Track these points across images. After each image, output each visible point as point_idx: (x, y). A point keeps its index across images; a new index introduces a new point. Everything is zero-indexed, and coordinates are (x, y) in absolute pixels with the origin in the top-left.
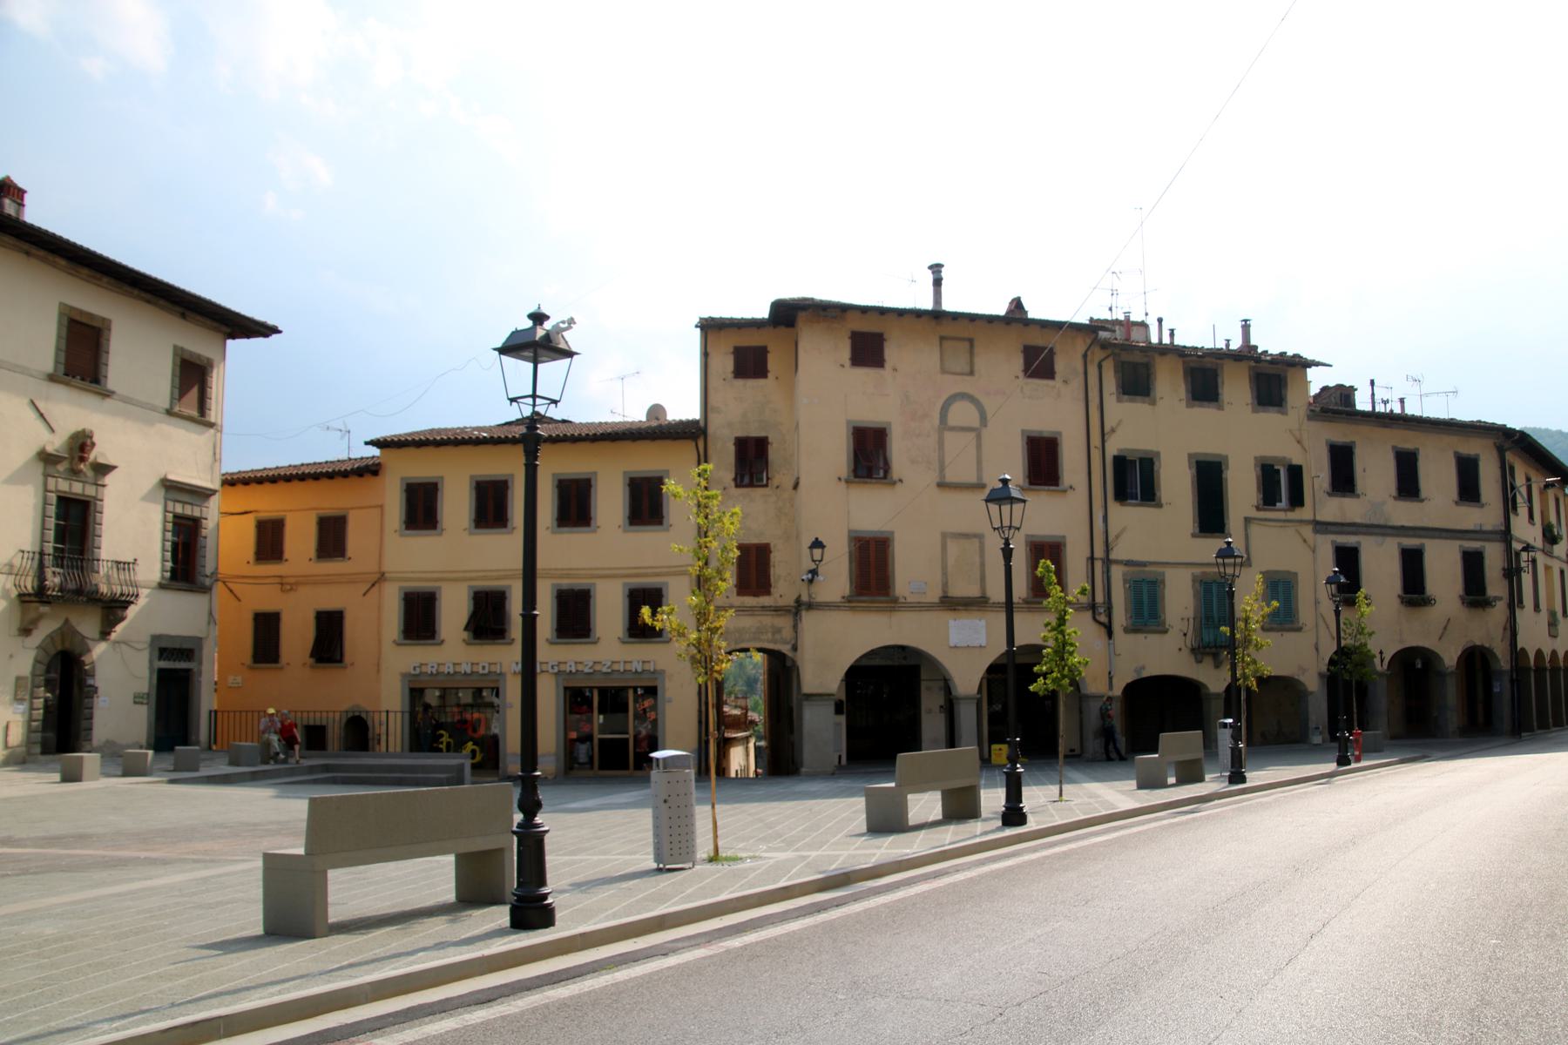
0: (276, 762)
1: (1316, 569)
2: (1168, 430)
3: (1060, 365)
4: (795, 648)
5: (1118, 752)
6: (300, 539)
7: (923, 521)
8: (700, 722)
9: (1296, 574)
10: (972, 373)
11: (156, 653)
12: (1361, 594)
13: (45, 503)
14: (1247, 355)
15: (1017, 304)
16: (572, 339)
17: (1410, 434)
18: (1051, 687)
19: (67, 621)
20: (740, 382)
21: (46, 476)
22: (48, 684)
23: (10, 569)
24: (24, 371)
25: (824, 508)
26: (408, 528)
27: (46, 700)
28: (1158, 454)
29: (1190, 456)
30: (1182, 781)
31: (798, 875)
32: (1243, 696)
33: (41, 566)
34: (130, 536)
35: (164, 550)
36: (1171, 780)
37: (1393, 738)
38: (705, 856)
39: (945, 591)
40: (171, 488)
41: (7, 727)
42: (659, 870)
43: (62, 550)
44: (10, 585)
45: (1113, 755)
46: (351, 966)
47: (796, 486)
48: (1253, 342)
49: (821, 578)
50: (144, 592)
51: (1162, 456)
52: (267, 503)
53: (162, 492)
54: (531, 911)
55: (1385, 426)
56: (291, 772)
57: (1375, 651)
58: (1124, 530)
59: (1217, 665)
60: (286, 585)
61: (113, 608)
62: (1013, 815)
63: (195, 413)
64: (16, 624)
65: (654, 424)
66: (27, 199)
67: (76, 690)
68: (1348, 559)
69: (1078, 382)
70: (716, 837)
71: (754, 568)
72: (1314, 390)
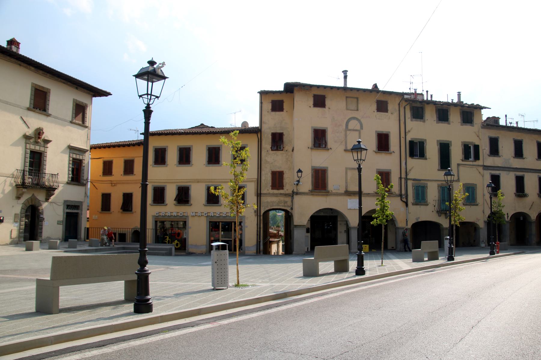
0: (106, 246)
1: (481, 181)
2: (430, 131)
3: (390, 107)
4: (292, 209)
5: (409, 248)
6: (118, 168)
7: (337, 163)
8: (257, 235)
9: (476, 185)
10: (357, 110)
11: (66, 207)
12: (499, 192)
13: (26, 153)
14: (460, 105)
15: (375, 86)
16: (165, 71)
17: (519, 134)
18: (379, 222)
19: (33, 195)
20: (274, 113)
21: (26, 143)
22: (26, 216)
23: (13, 176)
24: (18, 106)
25: (302, 158)
26: (155, 164)
27: (26, 222)
28: (426, 140)
29: (438, 141)
30: (430, 259)
31: (265, 293)
32: (454, 228)
33: (24, 175)
34: (56, 165)
35: (69, 171)
36: (426, 259)
37: (511, 245)
38: (234, 284)
39: (346, 189)
40: (72, 149)
41: (11, 231)
42: (213, 290)
43: (32, 170)
44: (13, 182)
45: (407, 249)
46: (53, 327)
47: (293, 150)
48: (462, 100)
49: (301, 183)
50: (61, 186)
51: (427, 141)
52: (107, 155)
53: (68, 150)
54: (142, 305)
55: (511, 131)
56: (111, 249)
57: (504, 213)
58: (412, 168)
59: (446, 218)
60: (113, 184)
61: (50, 191)
62: (360, 271)
63: (81, 123)
64: (15, 195)
65: (243, 128)
66: (21, 46)
67: (37, 219)
68: (496, 179)
69: (396, 114)
70: (238, 277)
71: (278, 179)
72: (484, 118)
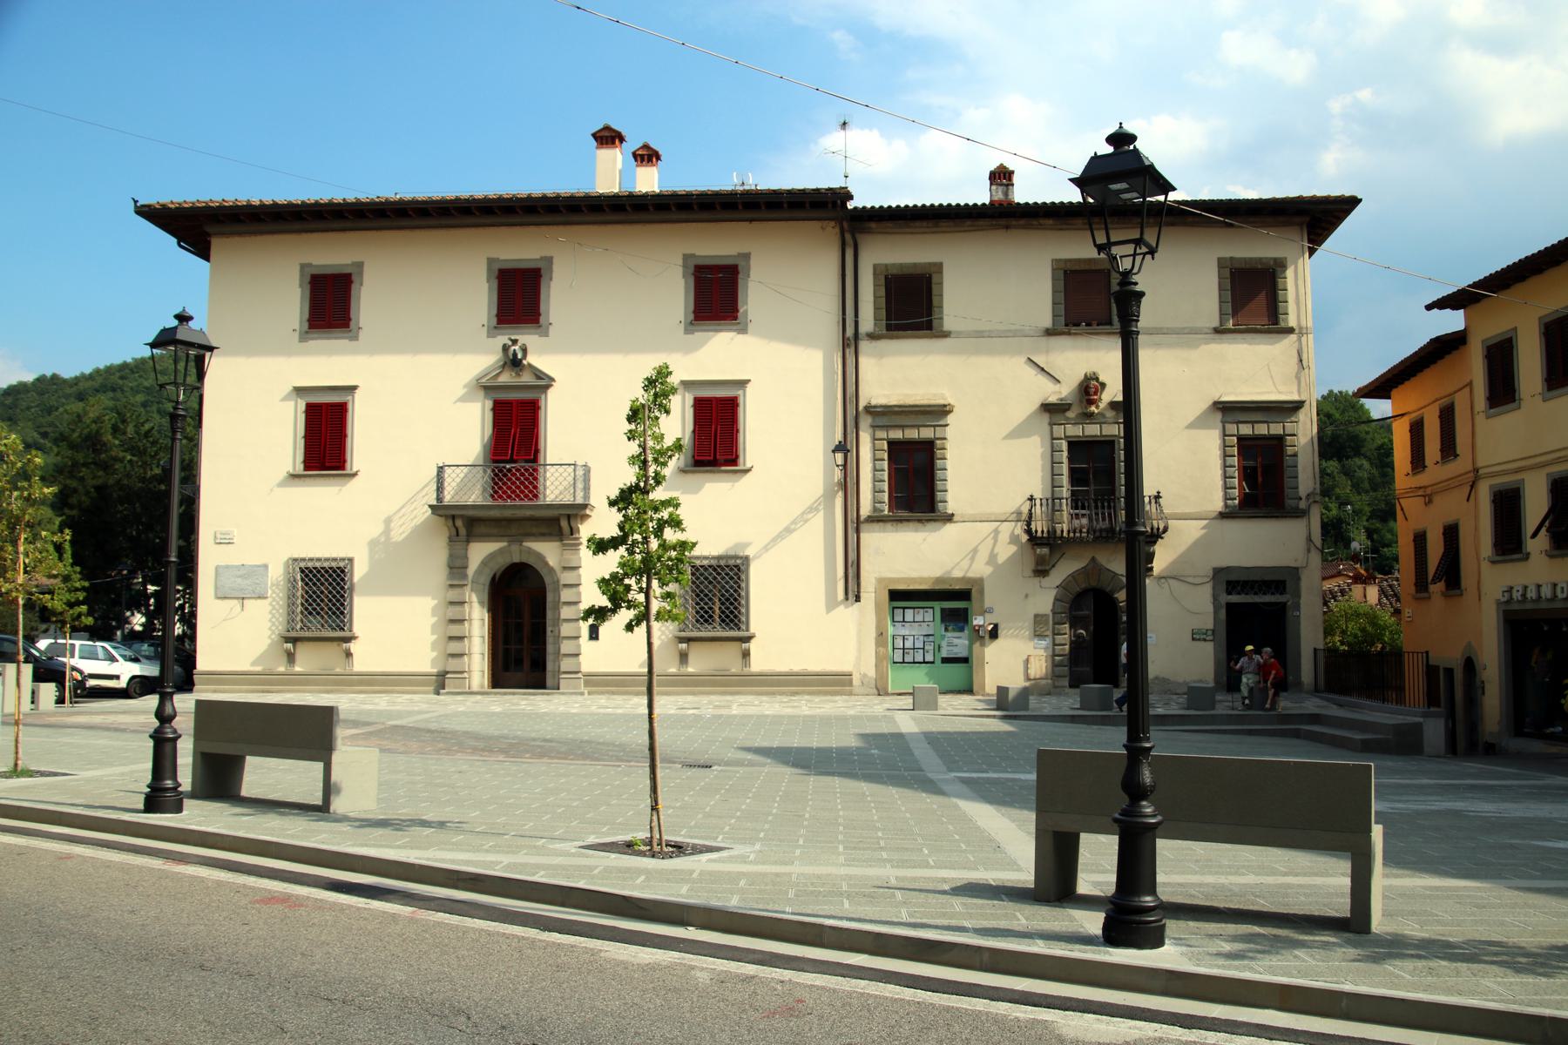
19: (1093, 559)
34: (1184, 472)
64: (1030, 565)
66: (1015, 179)
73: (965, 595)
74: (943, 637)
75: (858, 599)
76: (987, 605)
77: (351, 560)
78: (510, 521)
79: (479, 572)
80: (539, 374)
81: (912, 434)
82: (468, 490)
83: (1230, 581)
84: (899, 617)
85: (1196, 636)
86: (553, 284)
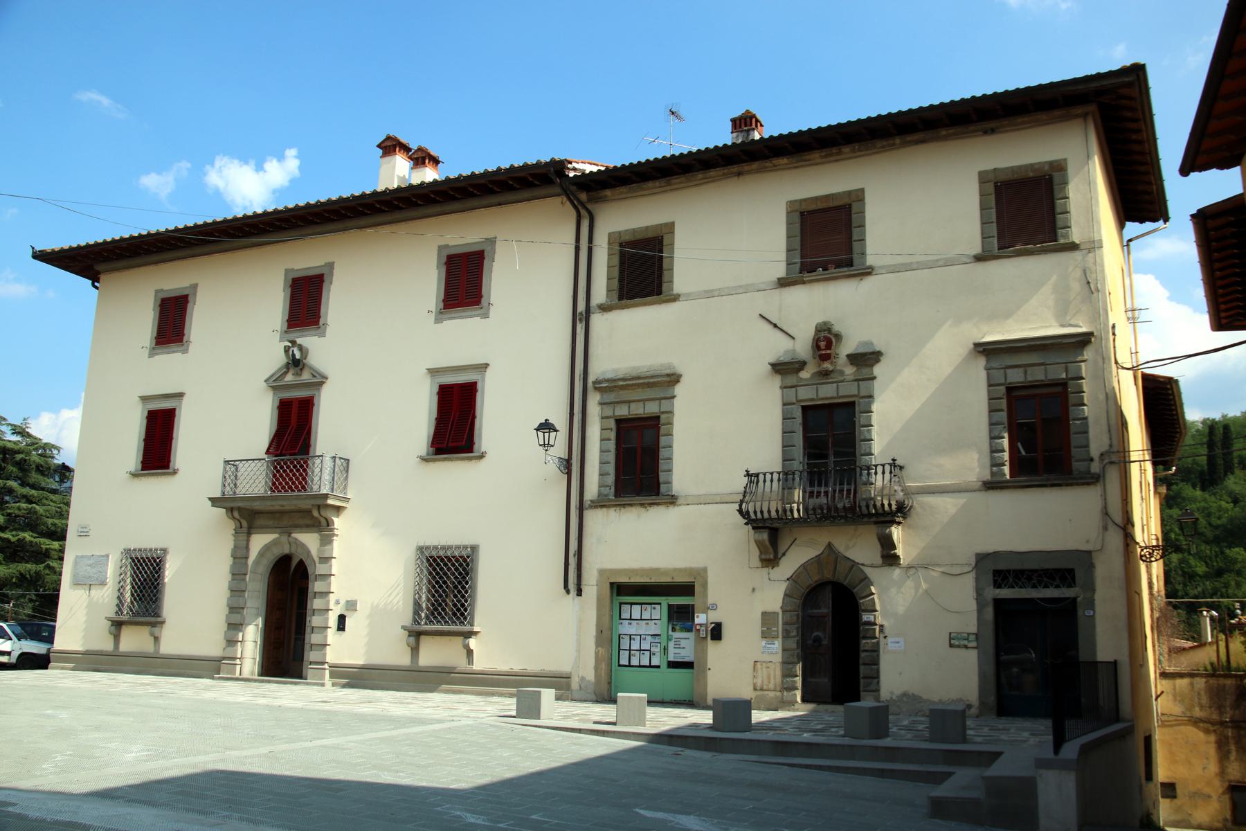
19: (830, 545)
73: (687, 589)
74: (669, 639)
75: (579, 592)
76: (710, 601)
77: (474, 549)
78: (283, 513)
79: (257, 562)
80: (315, 373)
81: (638, 410)
82: (255, 482)
83: (999, 571)
84: (625, 615)
85: (954, 642)
86: (333, 287)
